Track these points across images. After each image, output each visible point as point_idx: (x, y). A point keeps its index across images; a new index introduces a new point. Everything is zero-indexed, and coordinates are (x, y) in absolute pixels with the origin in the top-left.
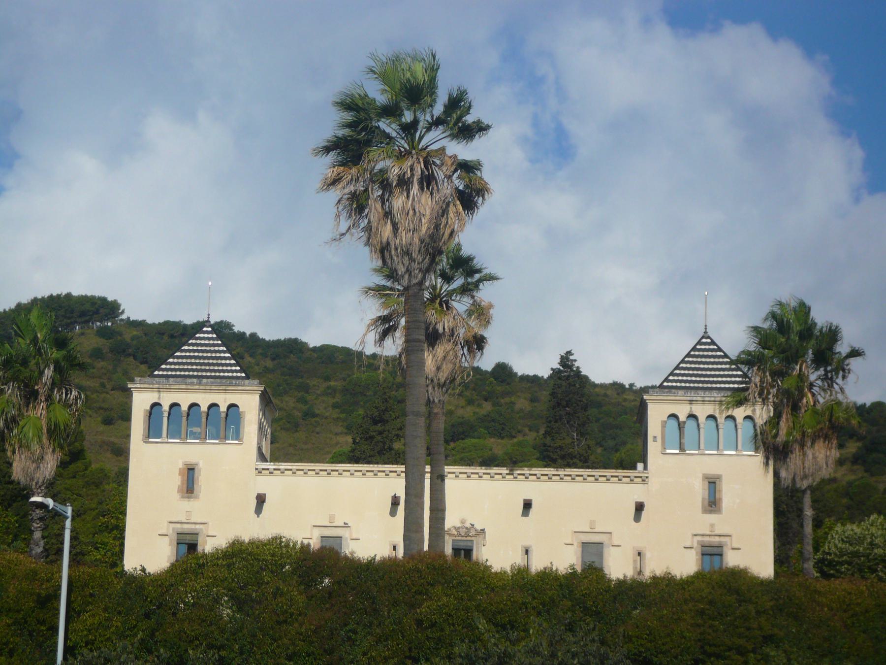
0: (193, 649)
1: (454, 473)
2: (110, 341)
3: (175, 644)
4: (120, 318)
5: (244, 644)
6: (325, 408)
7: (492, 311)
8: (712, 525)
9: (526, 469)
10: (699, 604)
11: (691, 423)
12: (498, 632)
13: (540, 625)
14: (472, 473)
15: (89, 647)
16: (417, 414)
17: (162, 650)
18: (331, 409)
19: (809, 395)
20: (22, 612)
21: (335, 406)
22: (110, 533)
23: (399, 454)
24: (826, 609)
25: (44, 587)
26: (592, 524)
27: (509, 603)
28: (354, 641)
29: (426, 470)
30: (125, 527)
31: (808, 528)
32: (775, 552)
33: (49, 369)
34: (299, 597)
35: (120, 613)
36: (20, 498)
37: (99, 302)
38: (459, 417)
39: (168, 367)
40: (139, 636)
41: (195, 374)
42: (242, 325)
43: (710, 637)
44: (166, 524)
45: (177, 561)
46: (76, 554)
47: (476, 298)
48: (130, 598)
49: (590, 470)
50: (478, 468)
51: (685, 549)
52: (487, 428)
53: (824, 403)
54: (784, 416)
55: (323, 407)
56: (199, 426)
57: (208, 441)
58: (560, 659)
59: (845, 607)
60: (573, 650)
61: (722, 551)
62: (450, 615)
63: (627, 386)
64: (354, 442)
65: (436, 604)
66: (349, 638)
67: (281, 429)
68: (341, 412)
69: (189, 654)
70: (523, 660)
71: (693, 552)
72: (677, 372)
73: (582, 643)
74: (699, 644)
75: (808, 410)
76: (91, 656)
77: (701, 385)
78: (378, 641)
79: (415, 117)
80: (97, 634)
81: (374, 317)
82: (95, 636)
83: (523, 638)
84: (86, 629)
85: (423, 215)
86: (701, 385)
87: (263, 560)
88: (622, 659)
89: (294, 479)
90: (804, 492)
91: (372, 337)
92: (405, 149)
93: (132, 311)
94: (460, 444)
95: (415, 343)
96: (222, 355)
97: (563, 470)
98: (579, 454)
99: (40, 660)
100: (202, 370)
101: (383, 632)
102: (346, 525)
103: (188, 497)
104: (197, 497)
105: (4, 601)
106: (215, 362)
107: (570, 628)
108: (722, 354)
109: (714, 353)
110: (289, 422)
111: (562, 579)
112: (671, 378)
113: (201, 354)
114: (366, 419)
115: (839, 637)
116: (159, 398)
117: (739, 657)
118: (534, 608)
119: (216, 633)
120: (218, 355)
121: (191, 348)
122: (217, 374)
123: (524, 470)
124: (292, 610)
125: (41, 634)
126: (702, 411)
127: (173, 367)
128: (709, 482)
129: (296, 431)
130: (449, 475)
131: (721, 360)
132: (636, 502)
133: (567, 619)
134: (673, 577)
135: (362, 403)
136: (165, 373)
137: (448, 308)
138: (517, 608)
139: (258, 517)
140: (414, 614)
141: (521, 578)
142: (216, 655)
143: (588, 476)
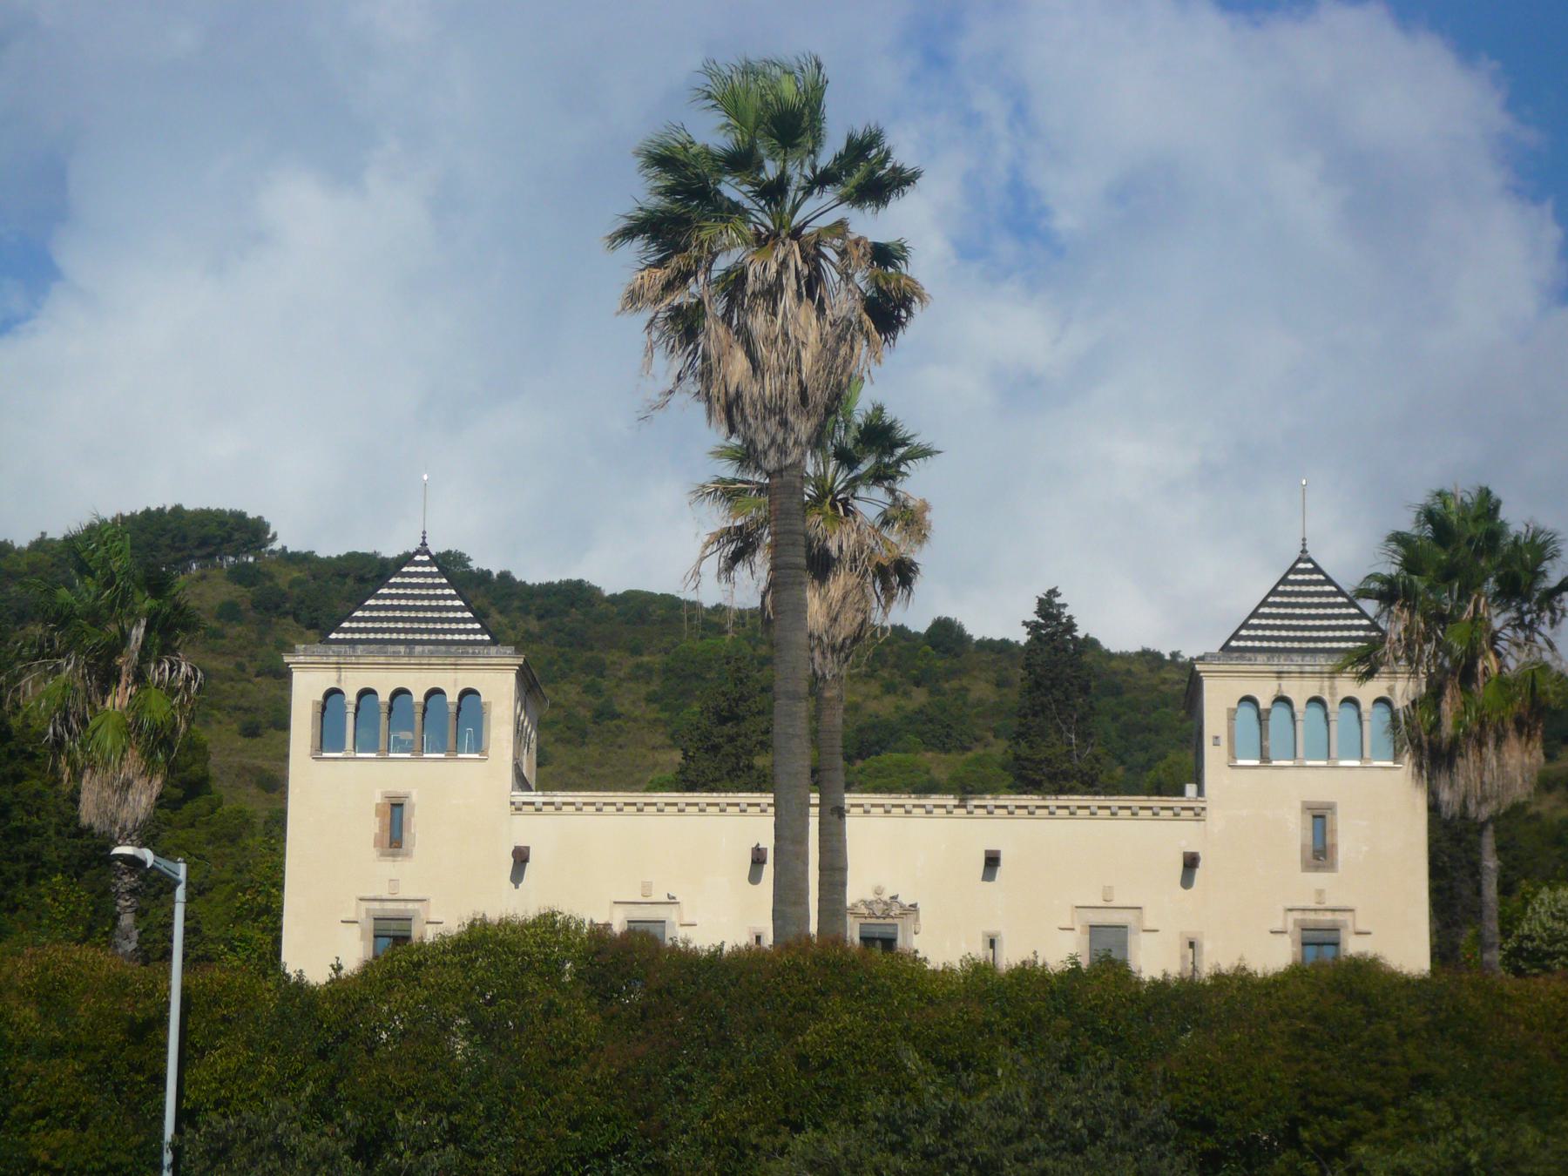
0: (404, 1112)
1: (861, 805)
2: (252, 589)
3: (372, 1104)
4: (269, 548)
5: (493, 1102)
6: (633, 703)
7: (928, 516)
8: (1320, 892)
9: (988, 797)
10: (1298, 1022)
11: (1280, 713)
12: (941, 1075)
13: (1015, 1062)
14: (894, 806)
15: (221, 1110)
16: (795, 697)
17: (348, 1114)
18: (643, 704)
19: (1492, 656)
20: (103, 1051)
21: (651, 699)
22: (255, 920)
23: (765, 776)
24: (1522, 1027)
25: (140, 1006)
26: (1107, 892)
27: (960, 1023)
28: (688, 1094)
29: (812, 802)
30: (282, 911)
31: (1491, 891)
32: (1431, 940)
33: (139, 625)
34: (589, 1019)
35: (273, 1050)
36: (95, 864)
37: (232, 521)
38: (871, 716)
39: (354, 625)
40: (308, 1090)
41: (402, 636)
42: (485, 560)
43: (1317, 1080)
44: (354, 903)
45: (376, 957)
46: (198, 959)
47: (897, 493)
48: (292, 1025)
49: (1103, 798)
50: (903, 796)
51: (1272, 935)
52: (920, 734)
53: (1518, 668)
54: (1448, 692)
55: (630, 699)
56: (411, 729)
57: (425, 756)
58: (1051, 1120)
59: (1556, 1022)
60: (1074, 1104)
61: (1339, 938)
62: (856, 1047)
63: (1168, 657)
64: (686, 756)
65: (830, 1027)
66: (679, 1090)
67: (556, 741)
68: (663, 710)
69: (397, 1121)
70: (985, 1123)
71: (1287, 939)
72: (1255, 621)
73: (1090, 1093)
74: (1298, 1091)
75: (1489, 681)
76: (224, 1125)
77: (1296, 645)
78: (730, 1094)
79: (783, 173)
80: (235, 1088)
81: (716, 529)
82: (232, 1091)
83: (986, 1085)
84: (215, 1078)
85: (803, 343)
86: (1296, 645)
87: (524, 953)
88: (1162, 1119)
89: (578, 820)
90: (1484, 825)
91: (713, 564)
92: (767, 229)
93: (289, 536)
94: (872, 762)
95: (788, 571)
96: (449, 603)
97: (1053, 797)
98: (1080, 771)
99: (135, 1134)
100: (414, 631)
101: (737, 1078)
102: (672, 901)
103: (393, 855)
104: (408, 855)
105: (70, 1031)
106: (436, 615)
107: (1069, 1066)
108: (1333, 589)
109: (1319, 588)
110: (569, 728)
111: (1054, 980)
112: (1244, 632)
113: (411, 603)
114: (705, 714)
115: (1545, 1077)
116: (339, 681)
117: (1369, 1114)
118: (1004, 1032)
119: (443, 1083)
120: (441, 603)
121: (393, 591)
122: (441, 637)
123: (984, 799)
124: (578, 1041)
125: (137, 1089)
126: (1299, 690)
127: (362, 625)
128: (1314, 817)
129: (583, 743)
130: (853, 810)
131: (1332, 600)
132: (1185, 853)
133: (1062, 1049)
134: (1250, 974)
135: (698, 693)
136: (349, 636)
137: (847, 512)
138: (975, 1033)
139: (517, 887)
140: (792, 1047)
141: (981, 980)
142: (445, 1123)
143: (1100, 808)
